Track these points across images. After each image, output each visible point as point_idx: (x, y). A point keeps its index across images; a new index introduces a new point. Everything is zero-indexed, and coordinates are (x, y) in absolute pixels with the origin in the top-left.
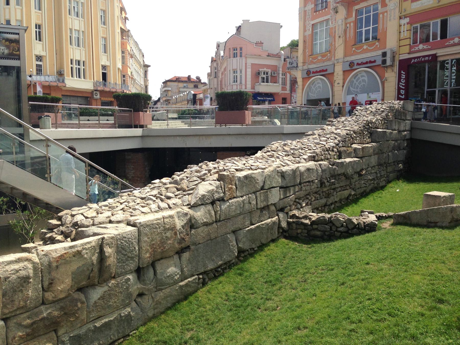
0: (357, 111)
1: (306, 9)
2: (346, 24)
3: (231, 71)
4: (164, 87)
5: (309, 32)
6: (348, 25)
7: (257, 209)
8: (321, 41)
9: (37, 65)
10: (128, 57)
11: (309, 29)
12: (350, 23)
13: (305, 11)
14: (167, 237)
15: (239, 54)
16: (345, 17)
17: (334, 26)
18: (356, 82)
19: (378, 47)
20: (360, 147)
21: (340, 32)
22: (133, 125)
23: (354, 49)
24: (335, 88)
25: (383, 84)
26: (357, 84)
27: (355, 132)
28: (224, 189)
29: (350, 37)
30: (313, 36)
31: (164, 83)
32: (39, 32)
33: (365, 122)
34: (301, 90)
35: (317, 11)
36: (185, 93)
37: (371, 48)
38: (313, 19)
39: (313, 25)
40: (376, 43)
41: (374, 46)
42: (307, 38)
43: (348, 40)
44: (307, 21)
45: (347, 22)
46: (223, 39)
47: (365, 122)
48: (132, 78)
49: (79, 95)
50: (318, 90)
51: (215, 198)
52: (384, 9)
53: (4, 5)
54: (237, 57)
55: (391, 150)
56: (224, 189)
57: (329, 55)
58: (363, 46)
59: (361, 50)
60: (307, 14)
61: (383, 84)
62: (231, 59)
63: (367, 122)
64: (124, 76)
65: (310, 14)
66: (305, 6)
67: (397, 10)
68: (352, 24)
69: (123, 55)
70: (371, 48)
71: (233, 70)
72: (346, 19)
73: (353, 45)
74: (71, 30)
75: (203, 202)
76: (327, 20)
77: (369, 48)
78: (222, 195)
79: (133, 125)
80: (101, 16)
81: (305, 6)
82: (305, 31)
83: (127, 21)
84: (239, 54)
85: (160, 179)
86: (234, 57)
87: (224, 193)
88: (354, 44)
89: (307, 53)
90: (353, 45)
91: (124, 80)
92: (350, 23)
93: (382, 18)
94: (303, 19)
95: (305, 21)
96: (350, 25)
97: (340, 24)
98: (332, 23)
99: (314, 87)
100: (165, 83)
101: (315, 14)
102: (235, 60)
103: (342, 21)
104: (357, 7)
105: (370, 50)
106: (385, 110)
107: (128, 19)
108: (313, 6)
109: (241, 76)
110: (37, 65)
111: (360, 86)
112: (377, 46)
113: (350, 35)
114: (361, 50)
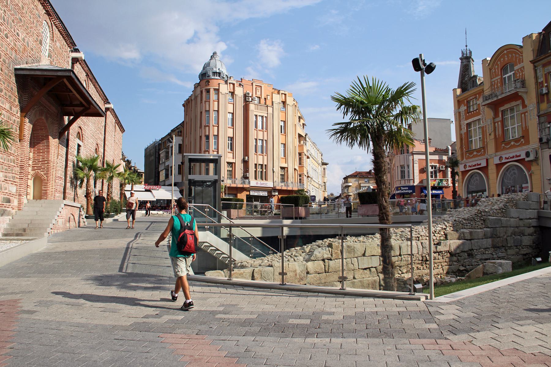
0: (481, 202)
1: (460, 110)
2: (495, 123)
3: (399, 167)
4: (345, 183)
5: (464, 130)
6: (496, 124)
7: (359, 269)
8: (475, 138)
9: (228, 170)
10: (305, 158)
11: (464, 128)
12: (498, 122)
13: (460, 113)
14: (290, 276)
15: (405, 151)
16: (493, 118)
17: (485, 125)
18: (508, 175)
19: (523, 143)
20: (468, 231)
21: (490, 130)
22: (294, 217)
23: (503, 145)
24: (490, 181)
25: (531, 176)
26: (509, 176)
27: (465, 219)
28: (332, 252)
29: (499, 135)
30: (468, 134)
31: (344, 178)
32: (231, 143)
33: (477, 211)
34: (461, 183)
35: (470, 112)
36: (365, 188)
37: (518, 144)
38: (466, 119)
39: (467, 124)
40: (521, 140)
41: (520, 142)
42: (463, 136)
43: (497, 137)
44: (462, 121)
45: (495, 121)
46: (461, 56)
47: (477, 211)
48: (308, 177)
49: (544, 60)
50: (476, 182)
51: (325, 257)
52: (525, 110)
53: (214, 175)
54: (404, 154)
55: (510, 235)
56: (332, 252)
57: (483, 150)
58: (511, 142)
59: (509, 146)
60: (461, 115)
61: (531, 176)
62: (399, 155)
63: (478, 211)
64: (300, 176)
65: (464, 114)
66: (459, 108)
67: (536, 110)
68: (499, 123)
69: (300, 157)
70: (518, 144)
71: (400, 166)
72: (494, 118)
73: (502, 142)
74: (256, 140)
75: (316, 259)
76: (479, 120)
77: (515, 144)
78: (330, 256)
79: (294, 217)
80: (281, 126)
81: (459, 108)
82: (461, 129)
83: (305, 126)
84: (405, 151)
85: (294, 247)
86: (402, 154)
87: (332, 255)
88: (503, 141)
89: (464, 149)
90: (502, 142)
91: (300, 179)
92: (498, 122)
93: (524, 118)
94: (458, 118)
95: (460, 121)
96: (498, 124)
97: (489, 123)
98: (483, 123)
99: (509, 173)
100: (346, 178)
101: (468, 115)
102: (402, 156)
103: (491, 121)
104: (502, 108)
105: (517, 146)
106: (503, 201)
107: (305, 125)
108: (465, 108)
109: (409, 172)
110: (228, 170)
111: (512, 178)
112: (522, 142)
113: (499, 133)
114: (509, 146)
